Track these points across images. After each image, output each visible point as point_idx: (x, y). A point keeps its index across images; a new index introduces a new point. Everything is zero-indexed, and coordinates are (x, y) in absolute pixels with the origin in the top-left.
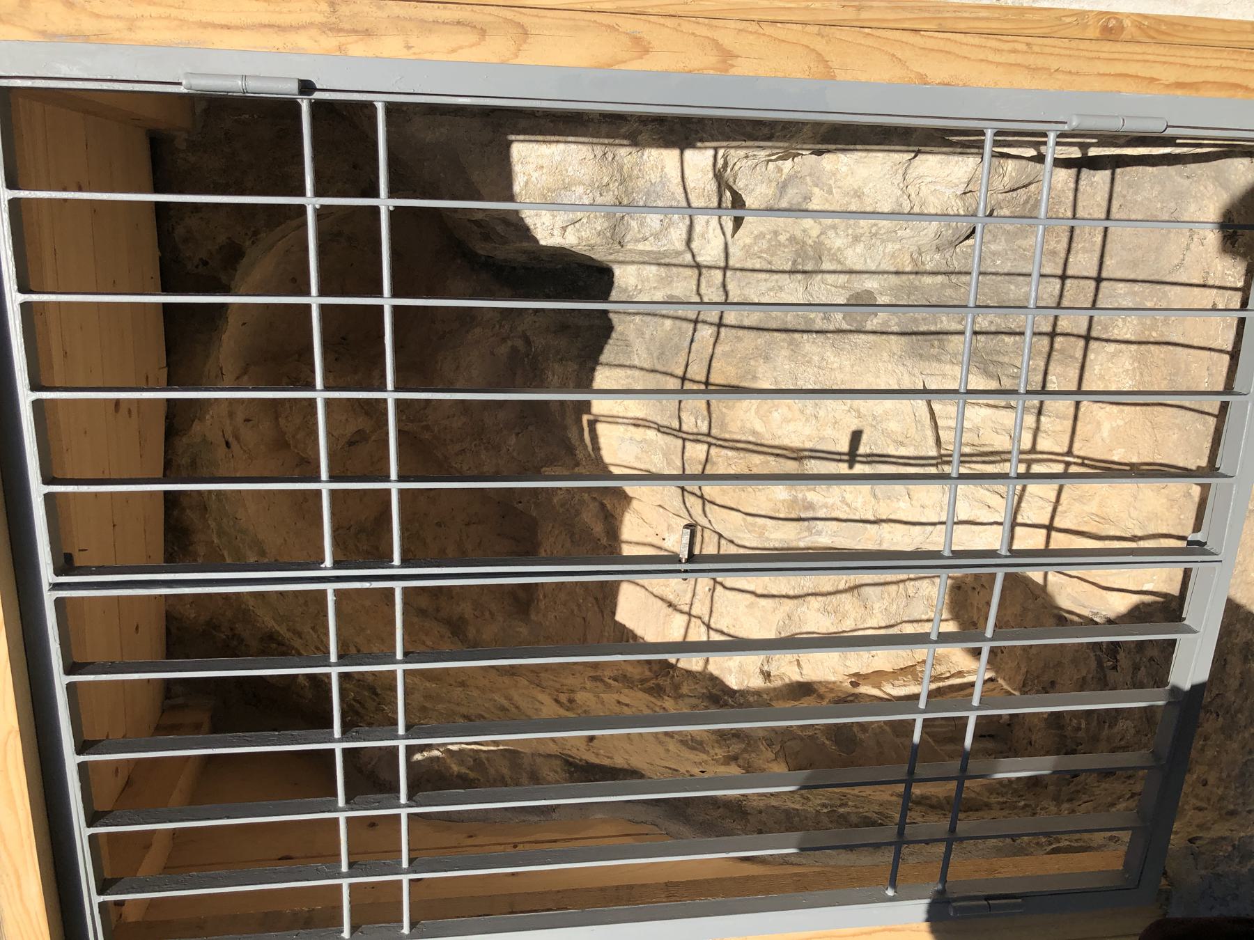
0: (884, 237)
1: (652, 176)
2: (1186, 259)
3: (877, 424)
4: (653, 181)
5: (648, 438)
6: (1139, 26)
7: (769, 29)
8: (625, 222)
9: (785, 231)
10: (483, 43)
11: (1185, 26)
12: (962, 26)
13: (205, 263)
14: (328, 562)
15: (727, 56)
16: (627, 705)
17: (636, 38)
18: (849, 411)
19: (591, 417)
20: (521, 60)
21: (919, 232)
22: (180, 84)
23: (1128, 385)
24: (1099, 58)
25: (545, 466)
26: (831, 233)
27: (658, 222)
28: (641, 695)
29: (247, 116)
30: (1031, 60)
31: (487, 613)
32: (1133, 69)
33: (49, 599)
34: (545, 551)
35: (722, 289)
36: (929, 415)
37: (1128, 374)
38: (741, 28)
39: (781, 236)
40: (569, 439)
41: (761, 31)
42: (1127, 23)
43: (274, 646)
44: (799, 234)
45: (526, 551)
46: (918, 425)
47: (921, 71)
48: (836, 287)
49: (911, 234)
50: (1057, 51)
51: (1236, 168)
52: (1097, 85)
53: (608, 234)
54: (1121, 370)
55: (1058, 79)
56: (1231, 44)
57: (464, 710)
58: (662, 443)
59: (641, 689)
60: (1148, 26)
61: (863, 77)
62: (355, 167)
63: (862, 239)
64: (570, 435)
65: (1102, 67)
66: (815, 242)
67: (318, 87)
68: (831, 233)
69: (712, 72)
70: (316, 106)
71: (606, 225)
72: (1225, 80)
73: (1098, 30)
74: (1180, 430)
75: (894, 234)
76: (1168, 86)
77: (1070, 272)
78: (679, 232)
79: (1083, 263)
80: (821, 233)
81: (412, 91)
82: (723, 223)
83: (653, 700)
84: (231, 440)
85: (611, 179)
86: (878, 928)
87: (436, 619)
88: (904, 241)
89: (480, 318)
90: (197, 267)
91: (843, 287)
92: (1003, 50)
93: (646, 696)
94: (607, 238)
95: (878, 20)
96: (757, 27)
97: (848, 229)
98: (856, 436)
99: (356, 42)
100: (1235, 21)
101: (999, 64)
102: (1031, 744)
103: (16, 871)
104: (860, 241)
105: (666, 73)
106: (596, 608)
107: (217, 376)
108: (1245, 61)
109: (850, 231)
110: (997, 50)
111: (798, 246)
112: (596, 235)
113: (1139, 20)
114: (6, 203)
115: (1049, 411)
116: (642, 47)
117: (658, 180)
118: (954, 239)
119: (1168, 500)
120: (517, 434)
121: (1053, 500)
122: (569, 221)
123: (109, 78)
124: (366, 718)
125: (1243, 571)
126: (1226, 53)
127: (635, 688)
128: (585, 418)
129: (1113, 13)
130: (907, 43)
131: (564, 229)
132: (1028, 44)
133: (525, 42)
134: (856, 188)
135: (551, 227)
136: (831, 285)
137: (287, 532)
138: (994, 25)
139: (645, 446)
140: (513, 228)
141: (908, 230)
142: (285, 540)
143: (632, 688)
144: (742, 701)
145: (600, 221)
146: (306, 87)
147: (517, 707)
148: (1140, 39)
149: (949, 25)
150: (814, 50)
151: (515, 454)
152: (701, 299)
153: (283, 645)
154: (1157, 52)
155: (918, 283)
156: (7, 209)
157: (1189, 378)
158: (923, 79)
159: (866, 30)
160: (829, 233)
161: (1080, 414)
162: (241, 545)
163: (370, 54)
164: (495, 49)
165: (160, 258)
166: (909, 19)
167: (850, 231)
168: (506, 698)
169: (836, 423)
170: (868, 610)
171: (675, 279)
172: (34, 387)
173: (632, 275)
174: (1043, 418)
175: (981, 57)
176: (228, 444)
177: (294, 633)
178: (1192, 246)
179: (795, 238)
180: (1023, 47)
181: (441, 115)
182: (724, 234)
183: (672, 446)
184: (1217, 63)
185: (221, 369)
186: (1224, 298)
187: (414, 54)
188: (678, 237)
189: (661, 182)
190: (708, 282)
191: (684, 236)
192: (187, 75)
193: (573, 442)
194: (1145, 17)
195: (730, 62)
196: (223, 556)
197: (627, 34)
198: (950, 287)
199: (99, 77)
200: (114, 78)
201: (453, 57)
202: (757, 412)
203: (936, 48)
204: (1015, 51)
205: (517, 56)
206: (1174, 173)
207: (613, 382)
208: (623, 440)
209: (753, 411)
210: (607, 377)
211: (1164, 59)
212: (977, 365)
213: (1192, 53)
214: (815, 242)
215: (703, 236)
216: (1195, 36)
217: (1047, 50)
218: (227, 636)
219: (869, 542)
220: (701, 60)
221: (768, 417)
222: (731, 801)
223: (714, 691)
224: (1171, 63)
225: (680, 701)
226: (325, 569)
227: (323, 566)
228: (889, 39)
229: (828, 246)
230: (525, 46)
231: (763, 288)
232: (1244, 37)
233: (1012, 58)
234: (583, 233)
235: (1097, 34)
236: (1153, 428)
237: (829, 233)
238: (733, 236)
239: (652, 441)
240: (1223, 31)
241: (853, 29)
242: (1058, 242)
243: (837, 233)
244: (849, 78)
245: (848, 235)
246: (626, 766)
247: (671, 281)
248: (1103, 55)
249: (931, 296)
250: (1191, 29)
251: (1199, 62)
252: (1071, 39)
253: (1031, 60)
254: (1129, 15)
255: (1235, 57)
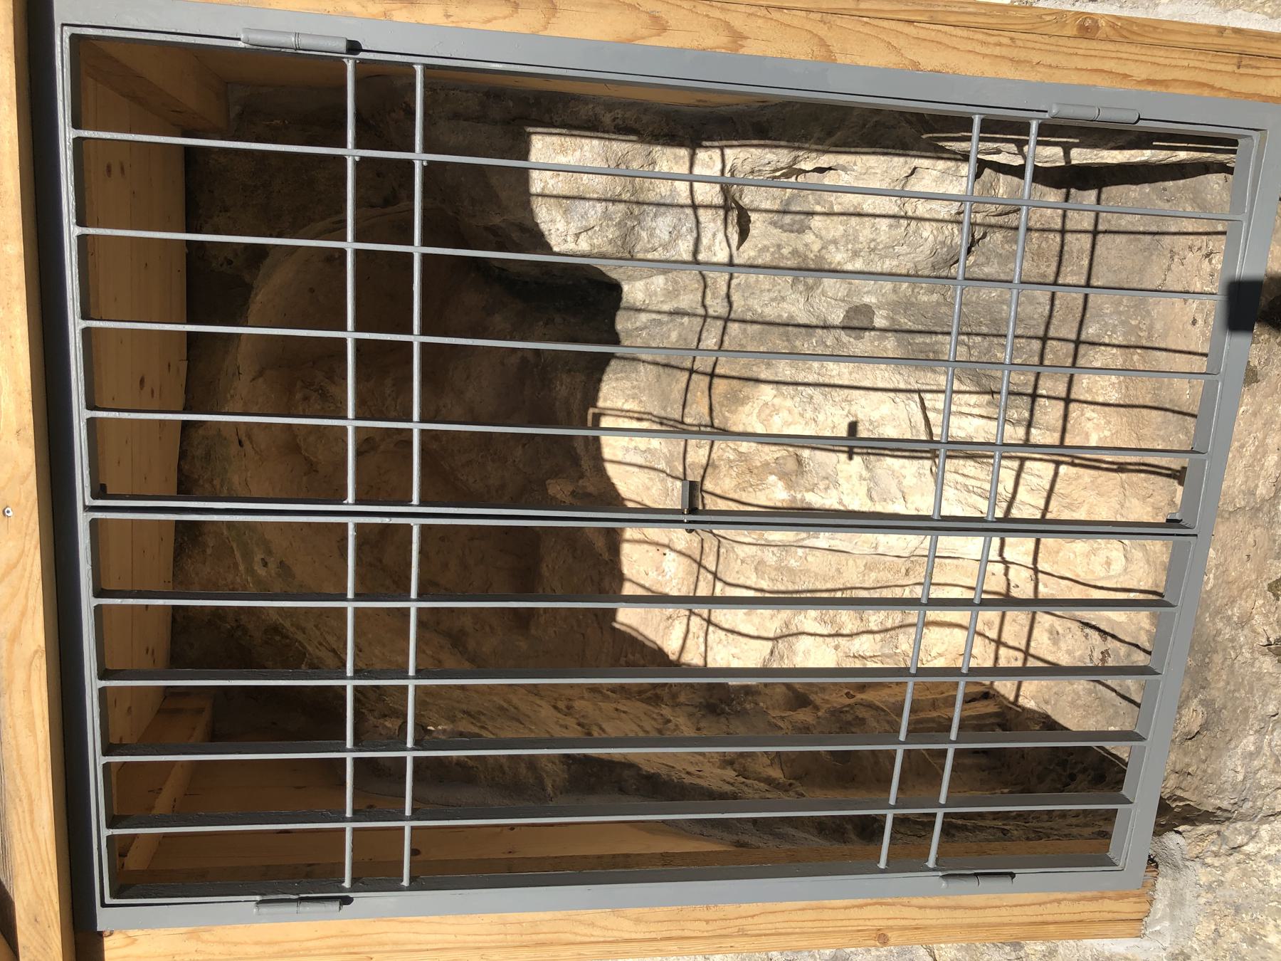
0: (883, 253)
1: (663, 189)
2: (1168, 279)
3: (874, 429)
4: (663, 195)
5: (652, 447)
6: (1113, 26)
7: (776, 15)
8: (636, 232)
9: (788, 245)
10: (515, 15)
11: (1155, 28)
12: (952, 19)
13: (230, 262)
14: (351, 497)
15: (738, 37)
16: (624, 712)
17: (655, 17)
18: (847, 416)
19: (596, 411)
20: (553, 32)
21: (915, 249)
22: (239, 39)
23: (1114, 398)
24: (1076, 54)
25: (549, 478)
26: (832, 248)
27: (667, 233)
28: (639, 704)
29: (279, 122)
30: (1014, 53)
31: (487, 629)
32: (1109, 65)
33: (83, 521)
34: (547, 566)
35: (726, 300)
36: (923, 421)
37: (1114, 387)
38: (751, 12)
39: (784, 250)
40: (575, 449)
41: (769, 16)
42: (1102, 23)
43: (278, 638)
44: (801, 248)
45: (526, 585)
46: (914, 431)
47: (915, 59)
48: (836, 300)
49: (908, 251)
50: (1038, 46)
51: (1212, 188)
52: (1075, 79)
53: (619, 243)
54: (1107, 383)
55: (1039, 72)
56: (1198, 46)
57: (464, 707)
58: (665, 450)
59: (638, 700)
60: (1121, 27)
61: (861, 62)
62: (378, 175)
63: (862, 254)
64: (576, 445)
65: (1081, 63)
66: (816, 256)
67: (364, 47)
68: (832, 248)
69: (723, 51)
70: (360, 65)
71: (617, 233)
72: (1192, 79)
73: (1075, 29)
74: (1164, 441)
75: (891, 250)
76: (1139, 82)
77: (1073, 396)
78: (686, 245)
79: (1072, 275)
80: (822, 248)
81: (449, 56)
82: (729, 235)
83: (651, 708)
84: (244, 439)
85: (623, 189)
86: (869, 901)
87: (435, 630)
88: (901, 258)
89: (491, 328)
90: (221, 265)
91: (843, 301)
92: (989, 43)
93: (644, 705)
94: (618, 246)
95: (876, 11)
96: (765, 12)
97: (848, 244)
98: (853, 427)
99: (401, 9)
100: (1201, 25)
101: (985, 56)
102: (1023, 757)
103: (30, 796)
104: (859, 256)
105: (682, 50)
106: (595, 625)
107: (234, 375)
108: (1210, 62)
109: (850, 246)
110: (983, 43)
111: (800, 259)
112: (608, 243)
113: (1113, 20)
114: (71, 141)
115: (1039, 424)
116: (660, 25)
117: (668, 193)
118: (949, 258)
119: (1154, 508)
120: (524, 445)
121: (1042, 506)
122: (582, 228)
123: (173, 31)
124: (367, 705)
125: (1224, 572)
126: (1193, 54)
127: (633, 699)
128: (591, 411)
129: (1089, 13)
130: (902, 33)
131: (577, 235)
132: (1012, 39)
133: (554, 16)
134: (856, 204)
135: (565, 233)
136: (831, 298)
137: (293, 537)
138: (981, 19)
139: (649, 456)
140: (528, 235)
141: (905, 247)
142: (291, 544)
143: (629, 699)
144: (739, 709)
145: (612, 229)
146: (354, 47)
147: (516, 708)
148: (1113, 38)
149: (940, 17)
150: (816, 35)
151: (521, 466)
152: (706, 311)
153: (287, 637)
154: (1128, 50)
155: (914, 300)
156: (71, 146)
157: (1172, 390)
158: (916, 64)
159: (865, 19)
160: (830, 247)
161: (1069, 426)
162: (249, 541)
163: (413, 21)
164: (525, 22)
165: (187, 255)
166: (904, 11)
167: (850, 246)
168: (505, 701)
169: (834, 427)
170: (864, 622)
171: (682, 292)
172: (85, 316)
173: (640, 290)
174: (1033, 430)
175: (970, 48)
176: (240, 443)
177: (298, 629)
178: (1173, 267)
179: (797, 252)
180: (1005, 41)
181: (465, 120)
182: (729, 246)
183: (675, 453)
184: (1185, 63)
185: (238, 368)
186: (1203, 313)
187: (453, 22)
188: (686, 248)
189: (670, 195)
190: (713, 294)
191: (691, 248)
192: (246, 30)
193: (578, 451)
194: (1119, 18)
195: (740, 43)
196: (232, 547)
197: (647, 13)
198: (945, 305)
199: (164, 30)
200: (178, 31)
201: (488, 27)
202: (759, 416)
203: (928, 38)
204: (1000, 44)
205: (546, 28)
206: (1155, 197)
207: (619, 392)
208: (627, 450)
209: (755, 415)
210: (614, 388)
211: (1136, 57)
212: (971, 377)
213: (1162, 53)
214: (816, 256)
215: (709, 248)
216: (1165, 37)
217: (1030, 45)
218: (232, 626)
219: (866, 545)
220: (713, 40)
221: (769, 420)
222: (726, 793)
223: (712, 701)
224: (1142, 61)
225: (677, 709)
226: (348, 504)
227: (345, 502)
228: (885, 28)
229: (829, 260)
230: (553, 20)
231: (766, 299)
232: (1209, 40)
233: (997, 51)
234: (595, 241)
235: (1075, 32)
236: (1139, 440)
237: (830, 247)
238: (738, 248)
239: (656, 449)
240: (1190, 34)
241: (853, 18)
242: (1048, 266)
243: (837, 248)
244: (848, 61)
245: (847, 250)
246: (623, 760)
247: (678, 295)
248: (1080, 52)
249: (927, 312)
250: (1159, 30)
251: (1167, 62)
252: (1050, 36)
253: (1014, 53)
254: (1103, 16)
255: (1201, 58)
